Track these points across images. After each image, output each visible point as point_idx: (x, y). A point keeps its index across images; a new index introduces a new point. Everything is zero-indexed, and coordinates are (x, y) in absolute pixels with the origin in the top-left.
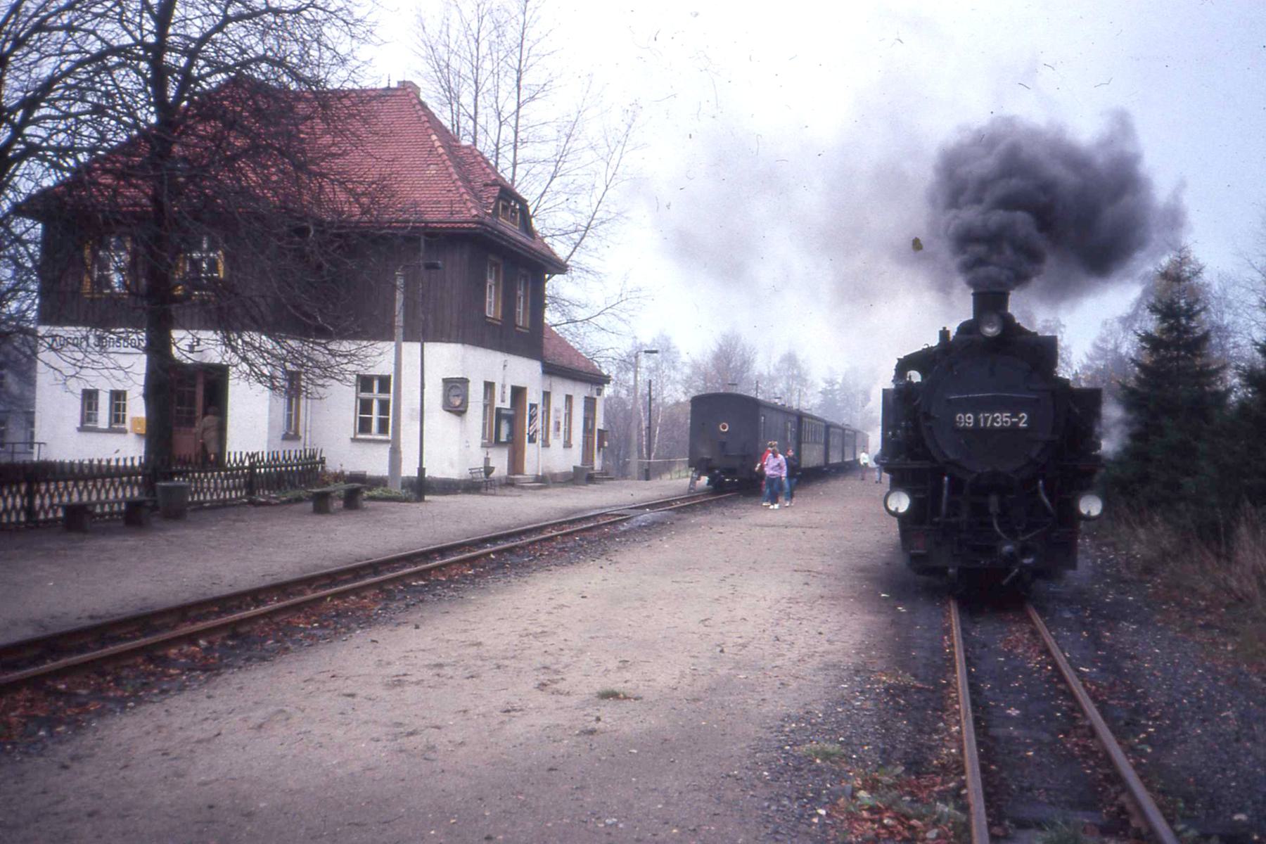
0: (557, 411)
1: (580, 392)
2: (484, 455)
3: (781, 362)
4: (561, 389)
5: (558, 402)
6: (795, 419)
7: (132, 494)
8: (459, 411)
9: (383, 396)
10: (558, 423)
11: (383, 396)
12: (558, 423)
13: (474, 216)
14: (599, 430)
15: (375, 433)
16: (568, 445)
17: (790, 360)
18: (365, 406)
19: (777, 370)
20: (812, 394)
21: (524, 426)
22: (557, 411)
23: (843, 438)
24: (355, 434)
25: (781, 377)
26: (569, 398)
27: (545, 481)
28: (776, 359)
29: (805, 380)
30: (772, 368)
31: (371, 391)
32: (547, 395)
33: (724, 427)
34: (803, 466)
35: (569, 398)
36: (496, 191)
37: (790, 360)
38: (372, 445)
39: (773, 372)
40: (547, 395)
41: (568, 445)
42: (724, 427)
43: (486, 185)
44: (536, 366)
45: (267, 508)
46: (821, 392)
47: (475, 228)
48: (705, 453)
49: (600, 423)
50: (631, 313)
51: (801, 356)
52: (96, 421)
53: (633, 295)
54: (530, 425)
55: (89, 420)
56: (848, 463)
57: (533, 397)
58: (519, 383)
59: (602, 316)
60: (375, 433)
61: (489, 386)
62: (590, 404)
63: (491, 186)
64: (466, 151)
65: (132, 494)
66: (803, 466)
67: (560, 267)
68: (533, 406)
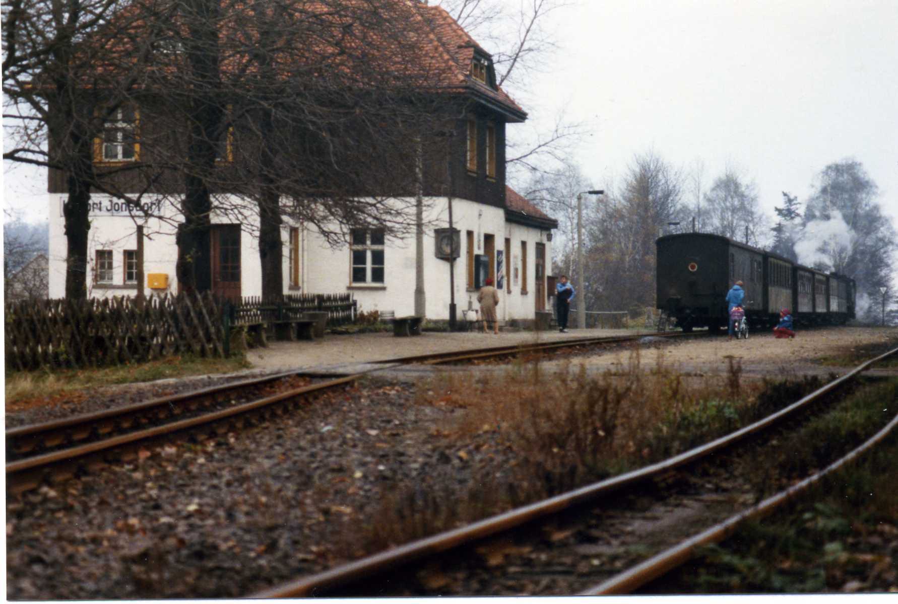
0: (516, 257)
1: (532, 237)
2: (467, 299)
3: (713, 189)
4: (520, 234)
5: (516, 250)
6: (760, 259)
7: (171, 340)
8: (450, 258)
9: (377, 247)
10: (516, 270)
11: (377, 247)
12: (516, 270)
13: (462, 81)
14: (549, 278)
15: (369, 282)
16: (524, 292)
17: (729, 185)
18: (358, 258)
19: (709, 200)
20: (762, 233)
21: (493, 272)
22: (516, 257)
23: (814, 285)
24: (350, 283)
25: (714, 210)
26: (524, 244)
27: (514, 325)
28: (707, 184)
29: (751, 213)
30: (702, 197)
31: (364, 243)
32: (507, 241)
33: (693, 267)
34: (770, 311)
35: (524, 244)
36: (470, 52)
37: (729, 185)
38: (367, 293)
39: (704, 204)
40: (507, 241)
41: (524, 292)
42: (693, 267)
43: (460, 47)
44: (500, 213)
45: (346, 336)
46: (774, 229)
47: (464, 93)
48: (673, 292)
49: (549, 272)
50: (568, 150)
51: (744, 180)
52: (112, 279)
53: (572, 131)
54: (498, 271)
55: (102, 278)
56: (820, 315)
57: (499, 245)
58: (490, 232)
59: (534, 155)
60: (369, 282)
61: (470, 234)
62: (541, 249)
63: (466, 47)
64: (433, 12)
65: (171, 340)
66: (770, 311)
67: (520, 116)
68: (500, 253)
